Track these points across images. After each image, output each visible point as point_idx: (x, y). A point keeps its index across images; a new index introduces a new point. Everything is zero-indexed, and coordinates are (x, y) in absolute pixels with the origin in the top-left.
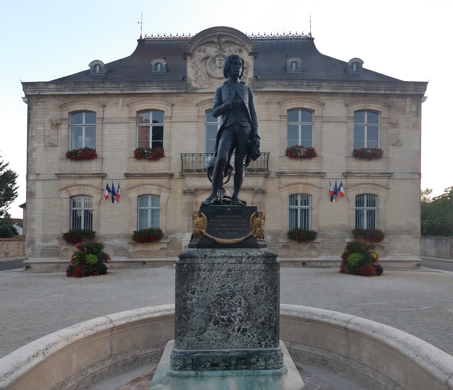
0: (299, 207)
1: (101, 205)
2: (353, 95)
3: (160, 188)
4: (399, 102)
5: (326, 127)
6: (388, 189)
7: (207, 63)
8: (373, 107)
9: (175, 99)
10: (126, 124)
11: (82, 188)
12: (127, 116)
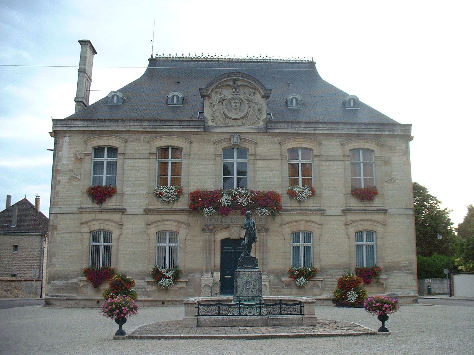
0: (301, 244)
1: (120, 240)
2: (347, 135)
3: (179, 225)
4: (391, 142)
5: (325, 165)
6: (384, 225)
7: (224, 104)
8: (367, 146)
9: (193, 138)
10: (147, 160)
11: (102, 222)
12: (148, 151)
